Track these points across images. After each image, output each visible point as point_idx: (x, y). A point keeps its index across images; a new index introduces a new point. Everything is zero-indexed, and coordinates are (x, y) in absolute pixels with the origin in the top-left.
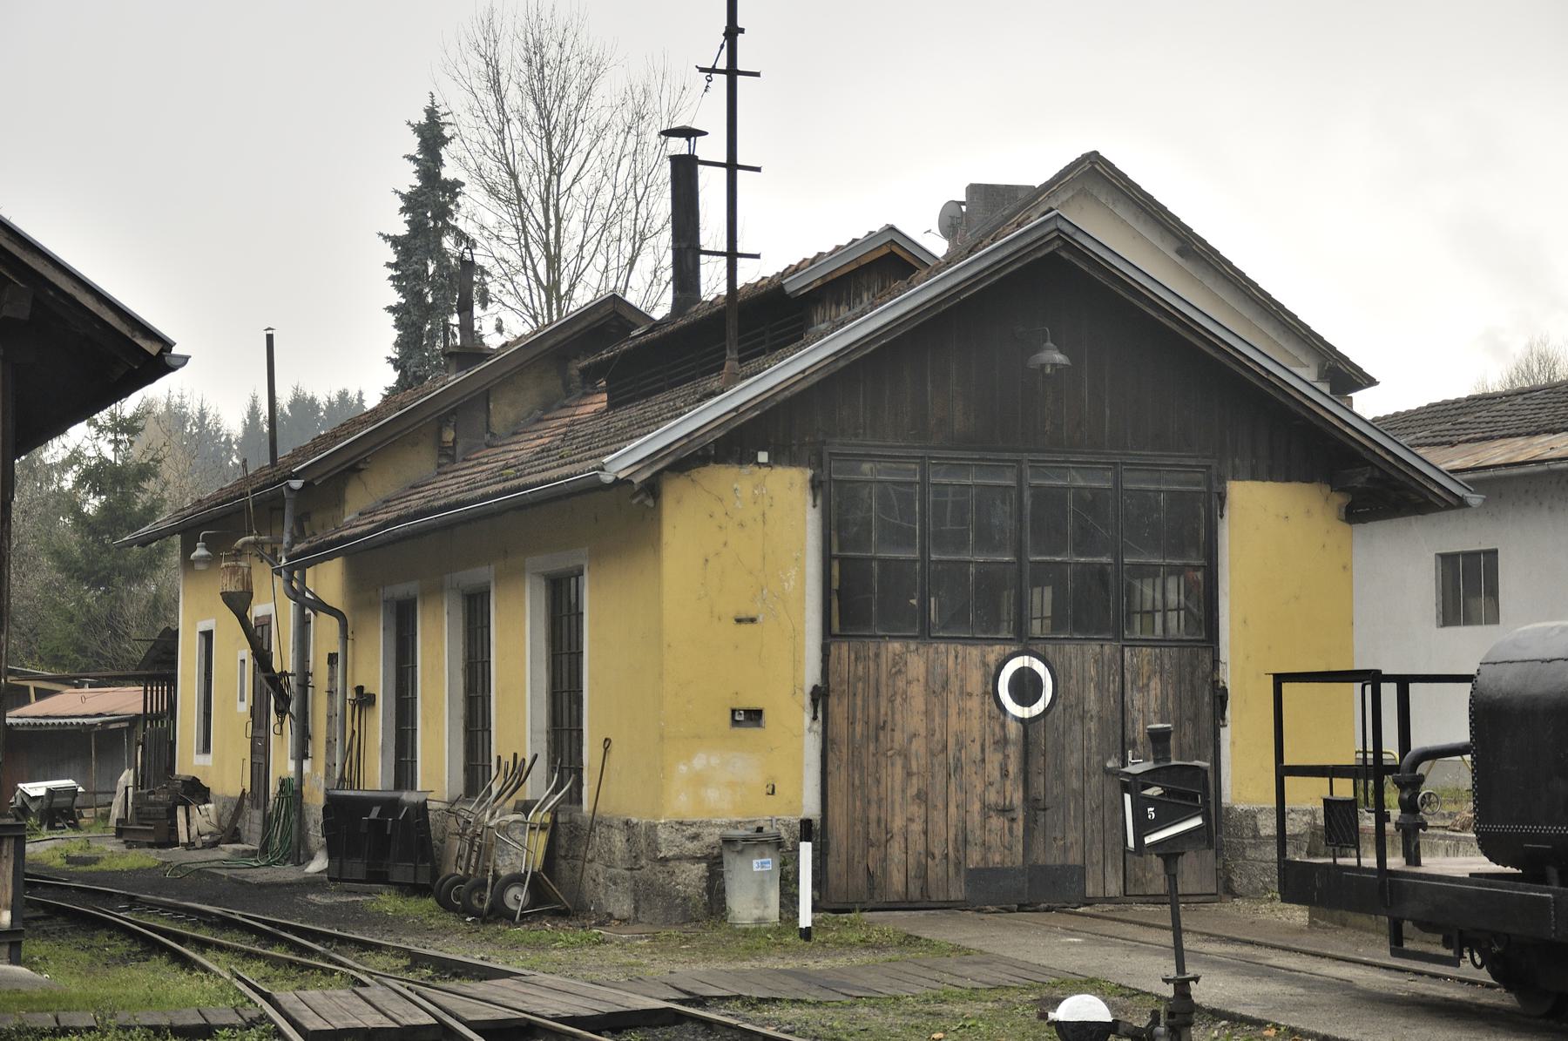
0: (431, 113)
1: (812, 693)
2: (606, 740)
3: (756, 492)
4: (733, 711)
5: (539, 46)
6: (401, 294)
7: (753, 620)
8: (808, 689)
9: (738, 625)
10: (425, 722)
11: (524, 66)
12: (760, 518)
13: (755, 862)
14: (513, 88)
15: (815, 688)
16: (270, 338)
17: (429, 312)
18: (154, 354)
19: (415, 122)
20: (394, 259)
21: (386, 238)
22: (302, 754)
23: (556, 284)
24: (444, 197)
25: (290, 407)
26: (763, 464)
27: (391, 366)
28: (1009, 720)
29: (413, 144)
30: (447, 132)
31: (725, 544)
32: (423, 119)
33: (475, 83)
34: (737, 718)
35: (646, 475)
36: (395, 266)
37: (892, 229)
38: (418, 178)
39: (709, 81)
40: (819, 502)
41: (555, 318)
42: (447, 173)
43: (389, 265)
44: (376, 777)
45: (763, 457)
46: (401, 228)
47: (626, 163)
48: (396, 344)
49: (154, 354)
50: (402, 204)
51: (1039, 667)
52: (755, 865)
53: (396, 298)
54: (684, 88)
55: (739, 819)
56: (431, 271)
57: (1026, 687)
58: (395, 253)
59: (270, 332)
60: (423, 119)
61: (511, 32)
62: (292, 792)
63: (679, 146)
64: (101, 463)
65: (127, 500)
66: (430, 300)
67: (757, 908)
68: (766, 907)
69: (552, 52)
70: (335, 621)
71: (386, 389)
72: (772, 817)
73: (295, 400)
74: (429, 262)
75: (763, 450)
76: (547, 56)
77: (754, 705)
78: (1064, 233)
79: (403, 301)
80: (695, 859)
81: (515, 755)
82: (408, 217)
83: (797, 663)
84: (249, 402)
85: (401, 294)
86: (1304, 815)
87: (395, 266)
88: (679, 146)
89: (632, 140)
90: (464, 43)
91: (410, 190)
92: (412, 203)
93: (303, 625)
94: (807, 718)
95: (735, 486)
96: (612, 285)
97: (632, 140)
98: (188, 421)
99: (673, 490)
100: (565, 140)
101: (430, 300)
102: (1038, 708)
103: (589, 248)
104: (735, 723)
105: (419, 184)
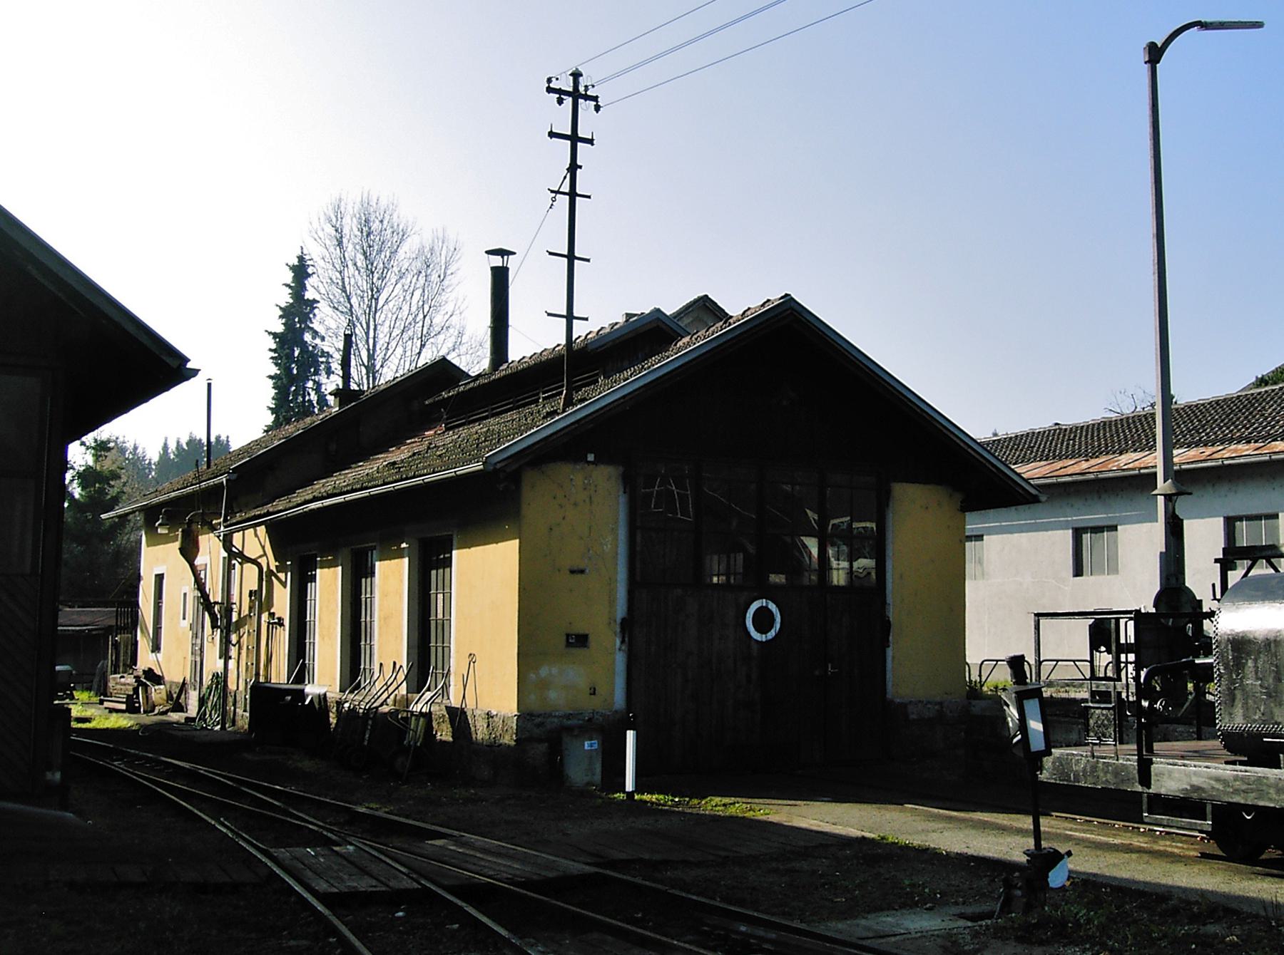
0: (301, 259)
1: (621, 623)
2: (471, 655)
3: (586, 481)
4: (568, 636)
5: (367, 221)
6: (277, 368)
7: (582, 572)
8: (619, 621)
9: (572, 575)
10: (322, 637)
11: (359, 234)
12: (588, 500)
13: (586, 743)
14: (350, 247)
15: (623, 620)
16: (209, 385)
17: (292, 379)
18: (175, 367)
19: (291, 264)
20: (274, 346)
21: (270, 333)
22: (225, 655)
23: (373, 365)
24: (306, 309)
25: (187, 444)
26: (590, 462)
27: (270, 412)
28: (753, 643)
29: (289, 277)
30: (310, 270)
31: (564, 518)
32: (296, 262)
33: (328, 242)
34: (570, 641)
35: (514, 467)
36: (274, 351)
37: (658, 310)
38: (291, 297)
39: (553, 201)
40: (627, 490)
41: (371, 386)
42: (309, 295)
43: (271, 350)
44: (279, 675)
45: (591, 457)
46: (279, 328)
47: (418, 293)
48: (273, 399)
49: (175, 367)
50: (281, 313)
51: (772, 607)
52: (586, 745)
53: (274, 370)
54: (455, 249)
55: (571, 712)
56: (296, 354)
57: (763, 621)
58: (275, 342)
59: (209, 381)
60: (296, 262)
61: (351, 213)
62: (220, 680)
63: (497, 261)
64: (87, 469)
65: (102, 492)
66: (295, 372)
67: (587, 776)
68: (594, 775)
69: (375, 226)
70: (256, 568)
71: (266, 426)
72: (594, 710)
73: (190, 440)
74: (296, 349)
75: (591, 453)
76: (372, 228)
77: (580, 628)
78: (796, 311)
79: (278, 372)
80: (540, 741)
81: (395, 663)
82: (284, 321)
83: (612, 602)
84: (163, 441)
85: (277, 368)
86: (936, 705)
87: (274, 351)
88: (497, 261)
89: (422, 279)
90: (322, 219)
91: (286, 305)
92: (287, 313)
93: (229, 568)
94: (618, 642)
95: (572, 477)
96: (407, 368)
97: (422, 279)
98: (127, 451)
99: (529, 477)
100: (382, 278)
101: (295, 372)
102: (771, 634)
103: (393, 344)
104: (568, 645)
105: (291, 301)
